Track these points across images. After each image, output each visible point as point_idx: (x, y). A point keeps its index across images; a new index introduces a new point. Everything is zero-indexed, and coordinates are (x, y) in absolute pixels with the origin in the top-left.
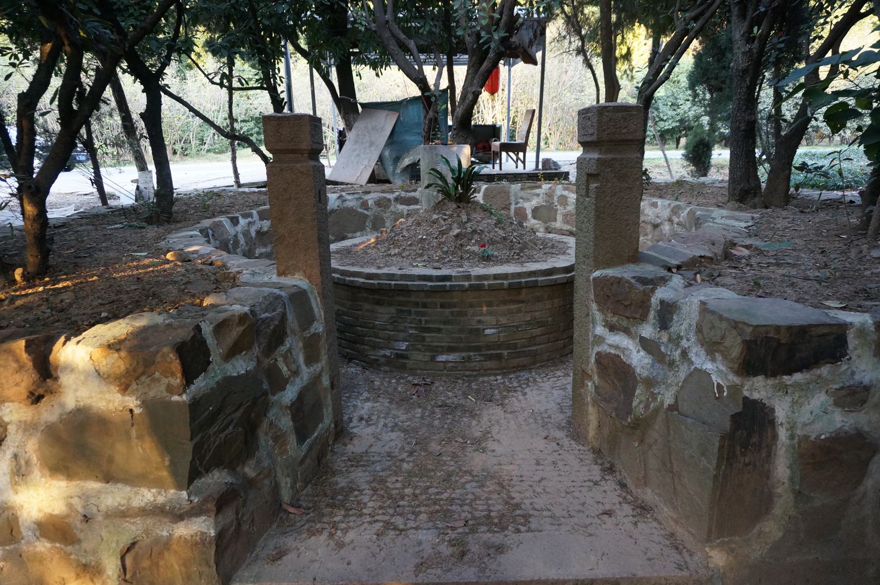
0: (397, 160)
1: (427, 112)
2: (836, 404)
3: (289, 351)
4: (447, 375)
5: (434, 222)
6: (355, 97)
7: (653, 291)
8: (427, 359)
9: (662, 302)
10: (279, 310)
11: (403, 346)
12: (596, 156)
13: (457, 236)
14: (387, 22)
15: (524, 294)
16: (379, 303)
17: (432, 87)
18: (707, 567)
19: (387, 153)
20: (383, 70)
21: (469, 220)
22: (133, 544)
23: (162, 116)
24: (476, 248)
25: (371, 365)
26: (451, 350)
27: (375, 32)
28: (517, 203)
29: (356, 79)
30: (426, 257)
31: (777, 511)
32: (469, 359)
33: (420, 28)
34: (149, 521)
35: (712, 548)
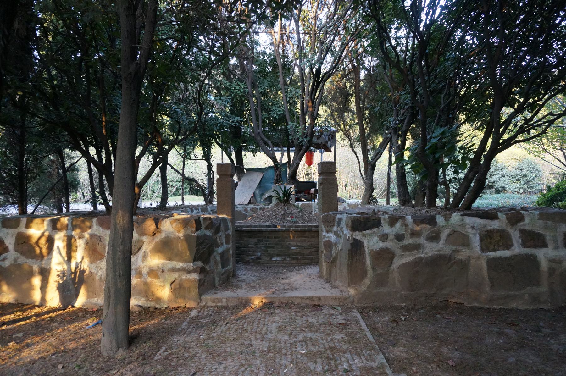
0: (262, 195)
1: (276, 172)
2: (380, 240)
3: (221, 236)
4: (276, 266)
5: (274, 210)
6: (243, 166)
7: (336, 216)
8: (268, 259)
9: (338, 218)
10: (219, 222)
11: (259, 254)
12: (322, 177)
13: (283, 215)
14: (259, 133)
15: (307, 234)
16: (250, 237)
17: (279, 161)
18: (348, 294)
19: (257, 192)
20: (257, 154)
21: (288, 210)
22: (175, 280)
23: (143, 177)
24: (290, 219)
25: (247, 263)
26: (278, 255)
27: (254, 137)
28: (315, 211)
29: (244, 158)
30: (270, 222)
31: (369, 276)
32: (285, 259)
33: (275, 135)
34: (180, 273)
35: (350, 288)
